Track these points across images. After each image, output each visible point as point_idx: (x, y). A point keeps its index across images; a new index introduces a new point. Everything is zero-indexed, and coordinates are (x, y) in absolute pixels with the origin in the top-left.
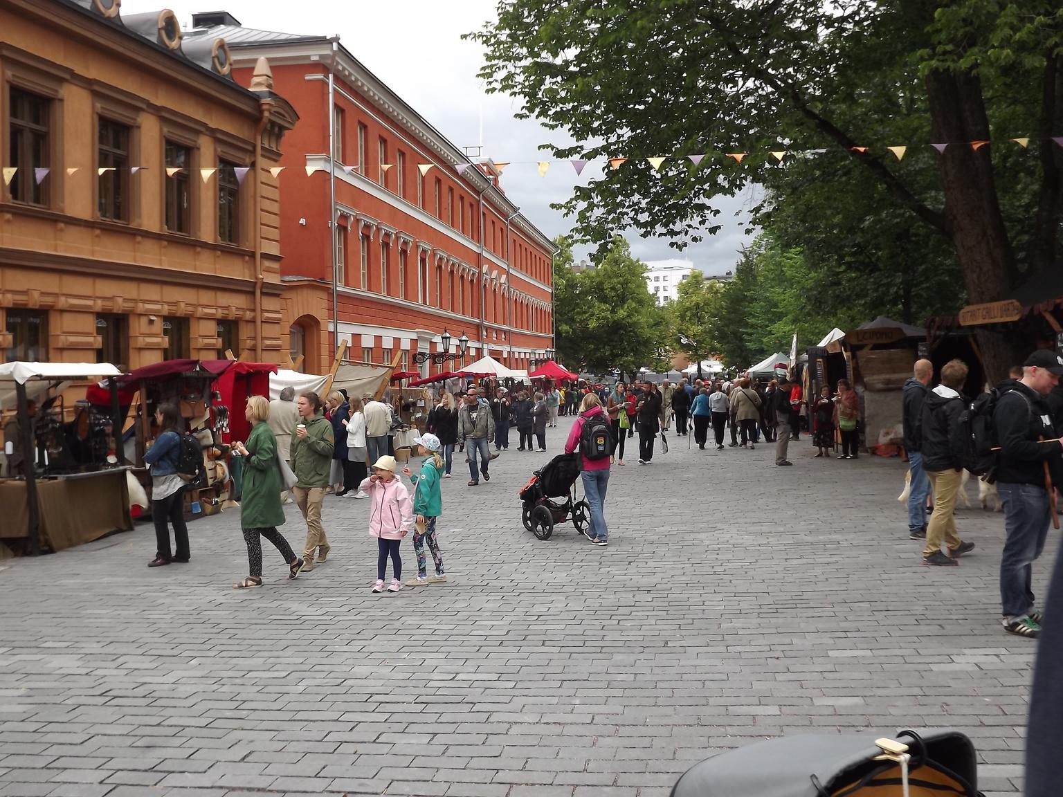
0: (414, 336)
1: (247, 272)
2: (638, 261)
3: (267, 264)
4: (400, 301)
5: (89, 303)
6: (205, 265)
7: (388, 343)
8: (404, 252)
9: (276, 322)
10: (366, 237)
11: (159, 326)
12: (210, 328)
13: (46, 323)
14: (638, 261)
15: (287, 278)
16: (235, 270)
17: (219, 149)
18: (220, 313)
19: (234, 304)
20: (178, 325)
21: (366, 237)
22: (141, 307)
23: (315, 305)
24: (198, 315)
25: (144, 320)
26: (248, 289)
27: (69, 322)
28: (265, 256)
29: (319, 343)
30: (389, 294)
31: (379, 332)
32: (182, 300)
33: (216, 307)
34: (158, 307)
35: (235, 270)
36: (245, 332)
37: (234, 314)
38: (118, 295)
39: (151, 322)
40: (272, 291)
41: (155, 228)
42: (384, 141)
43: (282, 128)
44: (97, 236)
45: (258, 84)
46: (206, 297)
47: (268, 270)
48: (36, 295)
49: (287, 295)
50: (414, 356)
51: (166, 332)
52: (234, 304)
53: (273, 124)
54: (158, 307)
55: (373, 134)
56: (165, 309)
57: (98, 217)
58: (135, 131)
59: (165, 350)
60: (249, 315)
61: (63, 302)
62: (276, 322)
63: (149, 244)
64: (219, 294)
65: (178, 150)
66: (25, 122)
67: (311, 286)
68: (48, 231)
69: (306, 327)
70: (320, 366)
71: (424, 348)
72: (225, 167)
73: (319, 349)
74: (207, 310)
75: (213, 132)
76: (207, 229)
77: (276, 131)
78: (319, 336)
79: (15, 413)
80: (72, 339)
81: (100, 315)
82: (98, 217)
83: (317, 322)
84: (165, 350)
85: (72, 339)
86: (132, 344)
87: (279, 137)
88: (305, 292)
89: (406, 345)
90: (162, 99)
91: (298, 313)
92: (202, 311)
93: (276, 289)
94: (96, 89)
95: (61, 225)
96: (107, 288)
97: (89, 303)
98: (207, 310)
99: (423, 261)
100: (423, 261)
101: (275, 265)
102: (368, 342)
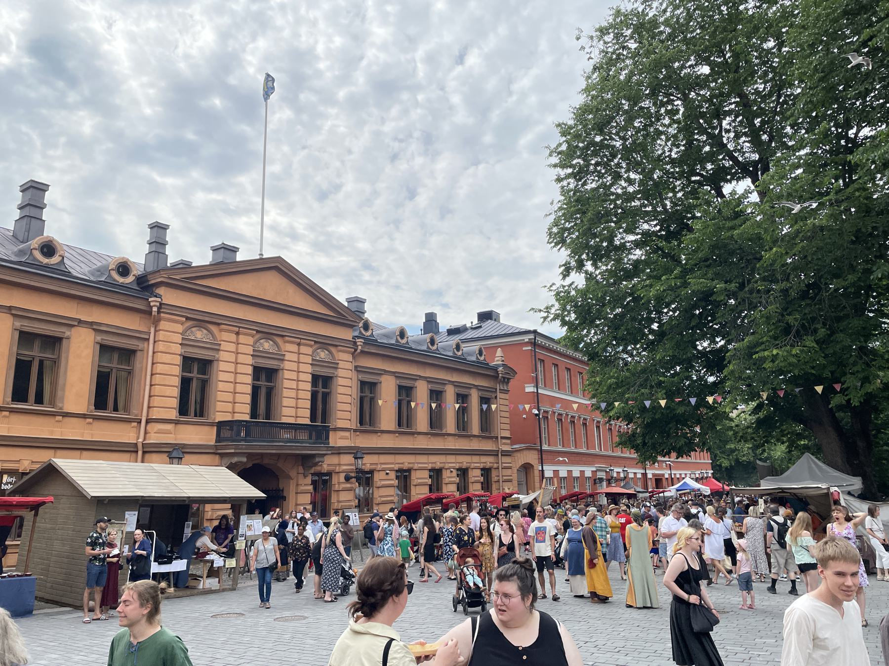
0: (594, 469)
1: (494, 446)
2: (431, 322)
3: (504, 441)
4: (584, 450)
5: (426, 465)
6: (475, 445)
7: (576, 474)
8: (585, 424)
9: (510, 468)
10: (560, 420)
11: (455, 473)
12: (478, 472)
13: (372, 477)
14: (431, 322)
15: (515, 446)
16: (488, 446)
17: (360, 377)
18: (482, 466)
19: (488, 461)
20: (436, 474)
21: (560, 420)
22: (447, 466)
23: (531, 458)
24: (415, 468)
25: (448, 471)
26: (494, 453)
27: (382, 475)
28: (502, 438)
29: (534, 476)
30: (576, 448)
31: (570, 468)
32: (437, 461)
33: (480, 463)
34: (454, 465)
35: (488, 446)
36: (494, 473)
37: (488, 465)
38: (405, 461)
39: (451, 471)
40: (506, 454)
41: (453, 432)
42: (568, 369)
43: (509, 379)
44: (90, 423)
45: (498, 361)
46: (476, 459)
47: (504, 444)
48: (406, 464)
49: (515, 454)
50: (595, 480)
51: (458, 475)
52: (488, 461)
53: (504, 378)
54: (454, 465)
55: (562, 367)
56: (457, 466)
57: (457, 432)
58: (444, 393)
59: (482, 483)
60: (495, 465)
61: (416, 466)
62: (510, 468)
63: (450, 438)
64: (482, 457)
65: (462, 398)
66: (404, 397)
67: (528, 449)
68: (410, 438)
69: (527, 468)
70: (534, 488)
71: (601, 475)
72: (485, 400)
73: (534, 479)
74: (476, 465)
75: (476, 387)
76: (475, 429)
77: (506, 381)
78: (533, 473)
79: (7, 543)
80: (419, 481)
81: (482, 469)
82: (457, 432)
83: (532, 466)
84: (482, 483)
85: (419, 481)
86: (444, 482)
87: (508, 383)
88: (525, 452)
89: (588, 474)
90: (456, 378)
91: (521, 462)
92: (473, 465)
93: (113, 446)
94: (397, 375)
95: (379, 434)
96: (484, 459)
97: (426, 465)
98: (476, 465)
99: (598, 427)
100: (598, 427)
101: (508, 441)
102: (563, 473)
